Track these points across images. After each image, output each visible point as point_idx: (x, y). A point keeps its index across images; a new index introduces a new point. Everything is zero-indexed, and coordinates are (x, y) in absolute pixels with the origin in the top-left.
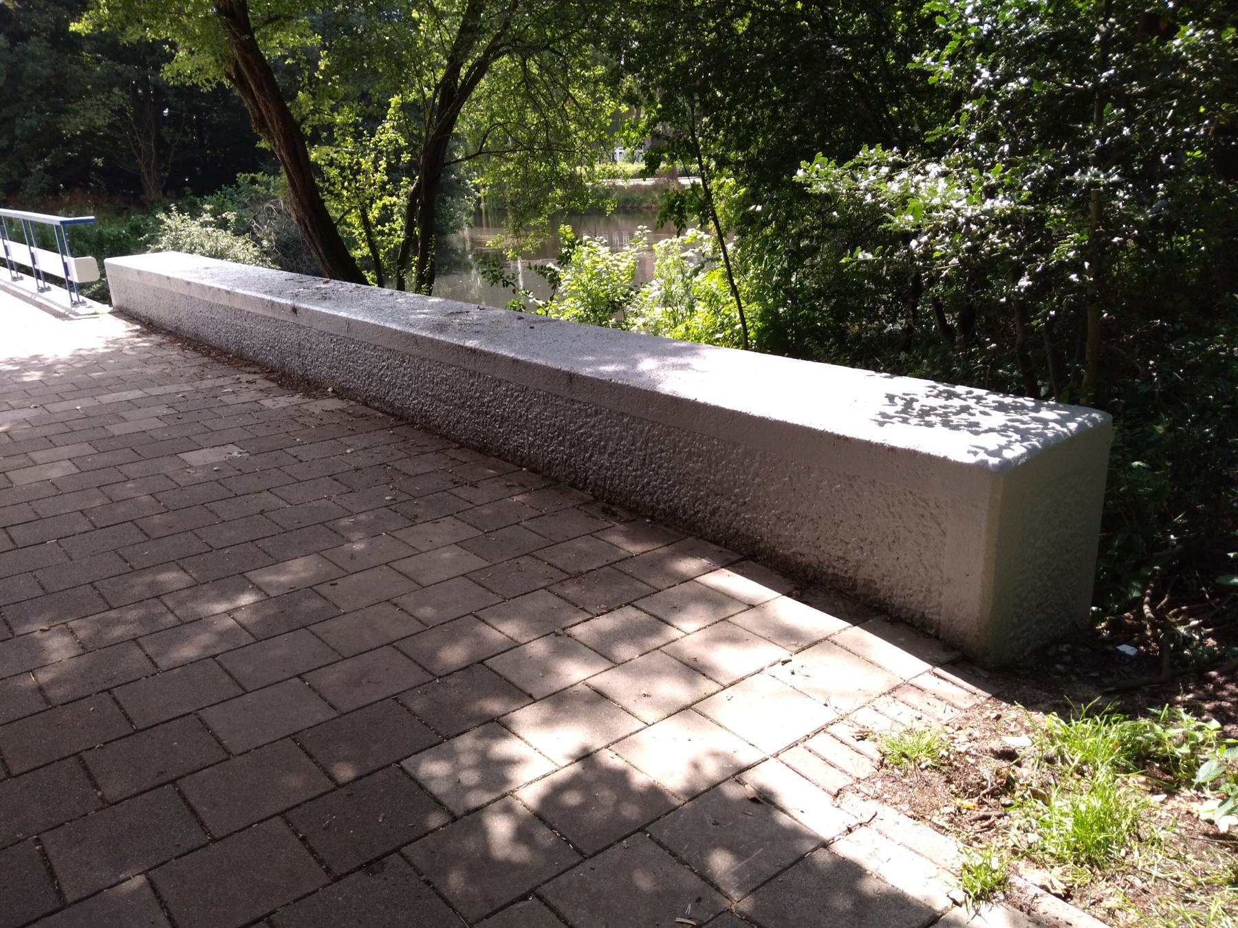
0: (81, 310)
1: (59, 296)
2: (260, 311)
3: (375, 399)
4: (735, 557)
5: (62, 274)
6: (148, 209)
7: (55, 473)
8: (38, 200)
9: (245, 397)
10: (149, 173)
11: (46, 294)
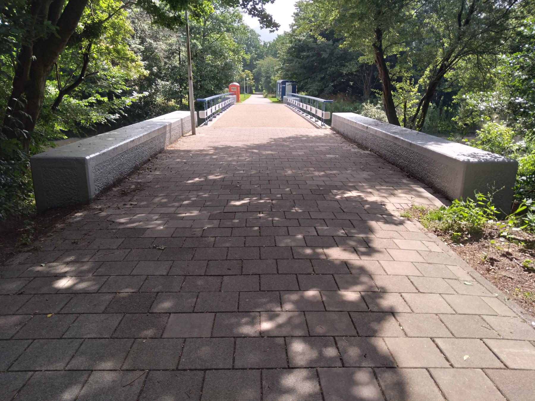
0: (323, 127)
1: (320, 123)
2: (361, 128)
3: (378, 152)
4: (426, 186)
5: (321, 116)
6: (362, 101)
7: (300, 153)
8: (327, 96)
9: (348, 148)
10: (366, 88)
11: (317, 123)
